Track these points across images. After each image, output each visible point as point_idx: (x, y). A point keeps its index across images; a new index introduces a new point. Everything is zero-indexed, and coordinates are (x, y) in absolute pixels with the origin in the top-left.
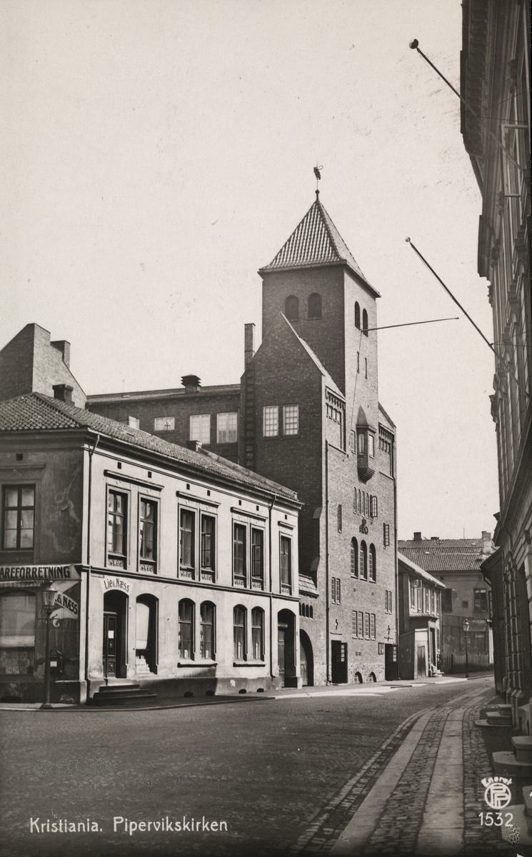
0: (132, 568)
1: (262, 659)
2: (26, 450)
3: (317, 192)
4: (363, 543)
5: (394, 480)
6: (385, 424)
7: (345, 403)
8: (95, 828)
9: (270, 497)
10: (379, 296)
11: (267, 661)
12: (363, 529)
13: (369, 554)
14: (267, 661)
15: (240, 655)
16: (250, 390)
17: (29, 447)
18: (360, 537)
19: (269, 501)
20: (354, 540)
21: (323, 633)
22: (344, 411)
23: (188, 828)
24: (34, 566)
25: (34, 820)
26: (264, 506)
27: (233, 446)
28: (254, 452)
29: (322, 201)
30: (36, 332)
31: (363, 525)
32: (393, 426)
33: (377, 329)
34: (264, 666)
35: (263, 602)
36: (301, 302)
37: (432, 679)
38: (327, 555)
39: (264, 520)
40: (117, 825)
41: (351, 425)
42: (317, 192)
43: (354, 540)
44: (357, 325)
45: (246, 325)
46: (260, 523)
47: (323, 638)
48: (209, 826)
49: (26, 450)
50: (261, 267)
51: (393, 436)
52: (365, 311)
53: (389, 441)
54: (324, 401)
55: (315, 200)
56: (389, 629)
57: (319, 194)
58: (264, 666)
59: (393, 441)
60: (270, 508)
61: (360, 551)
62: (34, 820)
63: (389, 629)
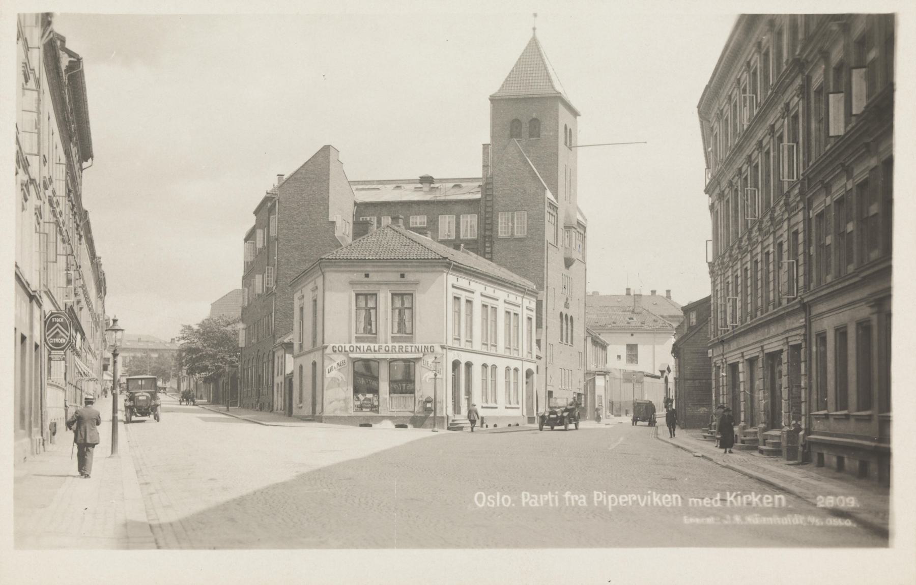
0: (463, 346)
1: (518, 403)
2: (407, 272)
3: (534, 29)
4: (566, 315)
5: (585, 263)
6: (581, 219)
7: (557, 208)
8: (768, 498)
9: (523, 290)
10: (579, 115)
11: (520, 405)
12: (567, 305)
13: (569, 323)
14: (520, 405)
15: (484, 401)
16: (488, 198)
17: (409, 269)
18: (565, 311)
19: (522, 292)
20: (561, 314)
21: (544, 385)
22: (557, 214)
23: (759, 502)
24: (400, 344)
25: (731, 496)
26: (513, 294)
27: (475, 241)
28: (491, 247)
29: (538, 36)
30: (331, 152)
31: (566, 303)
32: (586, 220)
33: (577, 147)
34: (518, 408)
35: (517, 364)
36: (524, 125)
37: (607, 420)
38: (547, 327)
39: (519, 307)
40: (612, 506)
41: (561, 225)
42: (534, 29)
43: (561, 314)
44: (566, 143)
45: (484, 145)
46: (517, 308)
47: (544, 389)
48: (761, 500)
49: (407, 272)
50: (491, 94)
51: (585, 228)
52: (570, 130)
53: (582, 232)
54: (547, 209)
55: (532, 36)
56: (580, 382)
57: (536, 31)
58: (518, 408)
59: (585, 232)
60: (523, 297)
61: (564, 321)
62: (731, 496)
63: (580, 382)
